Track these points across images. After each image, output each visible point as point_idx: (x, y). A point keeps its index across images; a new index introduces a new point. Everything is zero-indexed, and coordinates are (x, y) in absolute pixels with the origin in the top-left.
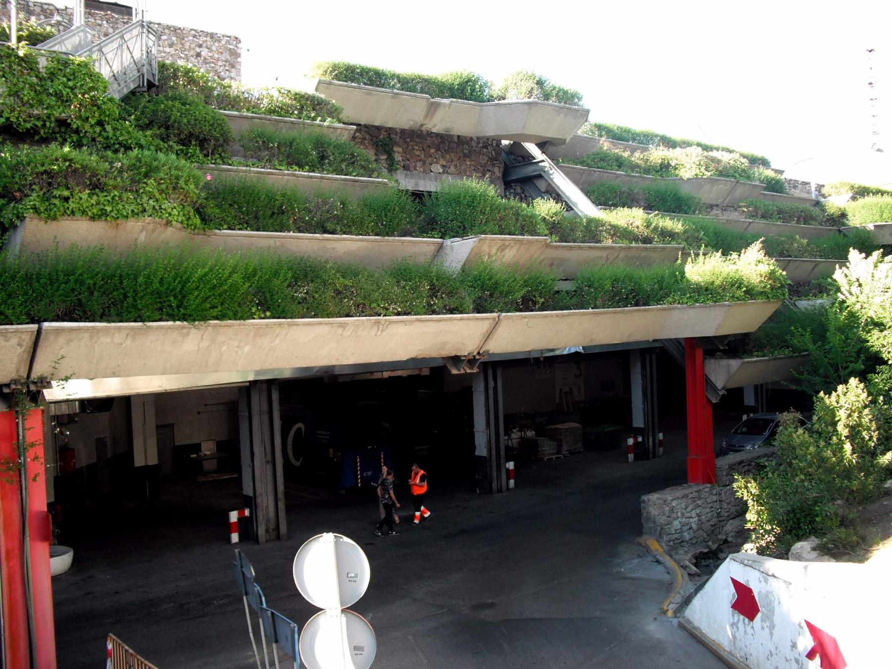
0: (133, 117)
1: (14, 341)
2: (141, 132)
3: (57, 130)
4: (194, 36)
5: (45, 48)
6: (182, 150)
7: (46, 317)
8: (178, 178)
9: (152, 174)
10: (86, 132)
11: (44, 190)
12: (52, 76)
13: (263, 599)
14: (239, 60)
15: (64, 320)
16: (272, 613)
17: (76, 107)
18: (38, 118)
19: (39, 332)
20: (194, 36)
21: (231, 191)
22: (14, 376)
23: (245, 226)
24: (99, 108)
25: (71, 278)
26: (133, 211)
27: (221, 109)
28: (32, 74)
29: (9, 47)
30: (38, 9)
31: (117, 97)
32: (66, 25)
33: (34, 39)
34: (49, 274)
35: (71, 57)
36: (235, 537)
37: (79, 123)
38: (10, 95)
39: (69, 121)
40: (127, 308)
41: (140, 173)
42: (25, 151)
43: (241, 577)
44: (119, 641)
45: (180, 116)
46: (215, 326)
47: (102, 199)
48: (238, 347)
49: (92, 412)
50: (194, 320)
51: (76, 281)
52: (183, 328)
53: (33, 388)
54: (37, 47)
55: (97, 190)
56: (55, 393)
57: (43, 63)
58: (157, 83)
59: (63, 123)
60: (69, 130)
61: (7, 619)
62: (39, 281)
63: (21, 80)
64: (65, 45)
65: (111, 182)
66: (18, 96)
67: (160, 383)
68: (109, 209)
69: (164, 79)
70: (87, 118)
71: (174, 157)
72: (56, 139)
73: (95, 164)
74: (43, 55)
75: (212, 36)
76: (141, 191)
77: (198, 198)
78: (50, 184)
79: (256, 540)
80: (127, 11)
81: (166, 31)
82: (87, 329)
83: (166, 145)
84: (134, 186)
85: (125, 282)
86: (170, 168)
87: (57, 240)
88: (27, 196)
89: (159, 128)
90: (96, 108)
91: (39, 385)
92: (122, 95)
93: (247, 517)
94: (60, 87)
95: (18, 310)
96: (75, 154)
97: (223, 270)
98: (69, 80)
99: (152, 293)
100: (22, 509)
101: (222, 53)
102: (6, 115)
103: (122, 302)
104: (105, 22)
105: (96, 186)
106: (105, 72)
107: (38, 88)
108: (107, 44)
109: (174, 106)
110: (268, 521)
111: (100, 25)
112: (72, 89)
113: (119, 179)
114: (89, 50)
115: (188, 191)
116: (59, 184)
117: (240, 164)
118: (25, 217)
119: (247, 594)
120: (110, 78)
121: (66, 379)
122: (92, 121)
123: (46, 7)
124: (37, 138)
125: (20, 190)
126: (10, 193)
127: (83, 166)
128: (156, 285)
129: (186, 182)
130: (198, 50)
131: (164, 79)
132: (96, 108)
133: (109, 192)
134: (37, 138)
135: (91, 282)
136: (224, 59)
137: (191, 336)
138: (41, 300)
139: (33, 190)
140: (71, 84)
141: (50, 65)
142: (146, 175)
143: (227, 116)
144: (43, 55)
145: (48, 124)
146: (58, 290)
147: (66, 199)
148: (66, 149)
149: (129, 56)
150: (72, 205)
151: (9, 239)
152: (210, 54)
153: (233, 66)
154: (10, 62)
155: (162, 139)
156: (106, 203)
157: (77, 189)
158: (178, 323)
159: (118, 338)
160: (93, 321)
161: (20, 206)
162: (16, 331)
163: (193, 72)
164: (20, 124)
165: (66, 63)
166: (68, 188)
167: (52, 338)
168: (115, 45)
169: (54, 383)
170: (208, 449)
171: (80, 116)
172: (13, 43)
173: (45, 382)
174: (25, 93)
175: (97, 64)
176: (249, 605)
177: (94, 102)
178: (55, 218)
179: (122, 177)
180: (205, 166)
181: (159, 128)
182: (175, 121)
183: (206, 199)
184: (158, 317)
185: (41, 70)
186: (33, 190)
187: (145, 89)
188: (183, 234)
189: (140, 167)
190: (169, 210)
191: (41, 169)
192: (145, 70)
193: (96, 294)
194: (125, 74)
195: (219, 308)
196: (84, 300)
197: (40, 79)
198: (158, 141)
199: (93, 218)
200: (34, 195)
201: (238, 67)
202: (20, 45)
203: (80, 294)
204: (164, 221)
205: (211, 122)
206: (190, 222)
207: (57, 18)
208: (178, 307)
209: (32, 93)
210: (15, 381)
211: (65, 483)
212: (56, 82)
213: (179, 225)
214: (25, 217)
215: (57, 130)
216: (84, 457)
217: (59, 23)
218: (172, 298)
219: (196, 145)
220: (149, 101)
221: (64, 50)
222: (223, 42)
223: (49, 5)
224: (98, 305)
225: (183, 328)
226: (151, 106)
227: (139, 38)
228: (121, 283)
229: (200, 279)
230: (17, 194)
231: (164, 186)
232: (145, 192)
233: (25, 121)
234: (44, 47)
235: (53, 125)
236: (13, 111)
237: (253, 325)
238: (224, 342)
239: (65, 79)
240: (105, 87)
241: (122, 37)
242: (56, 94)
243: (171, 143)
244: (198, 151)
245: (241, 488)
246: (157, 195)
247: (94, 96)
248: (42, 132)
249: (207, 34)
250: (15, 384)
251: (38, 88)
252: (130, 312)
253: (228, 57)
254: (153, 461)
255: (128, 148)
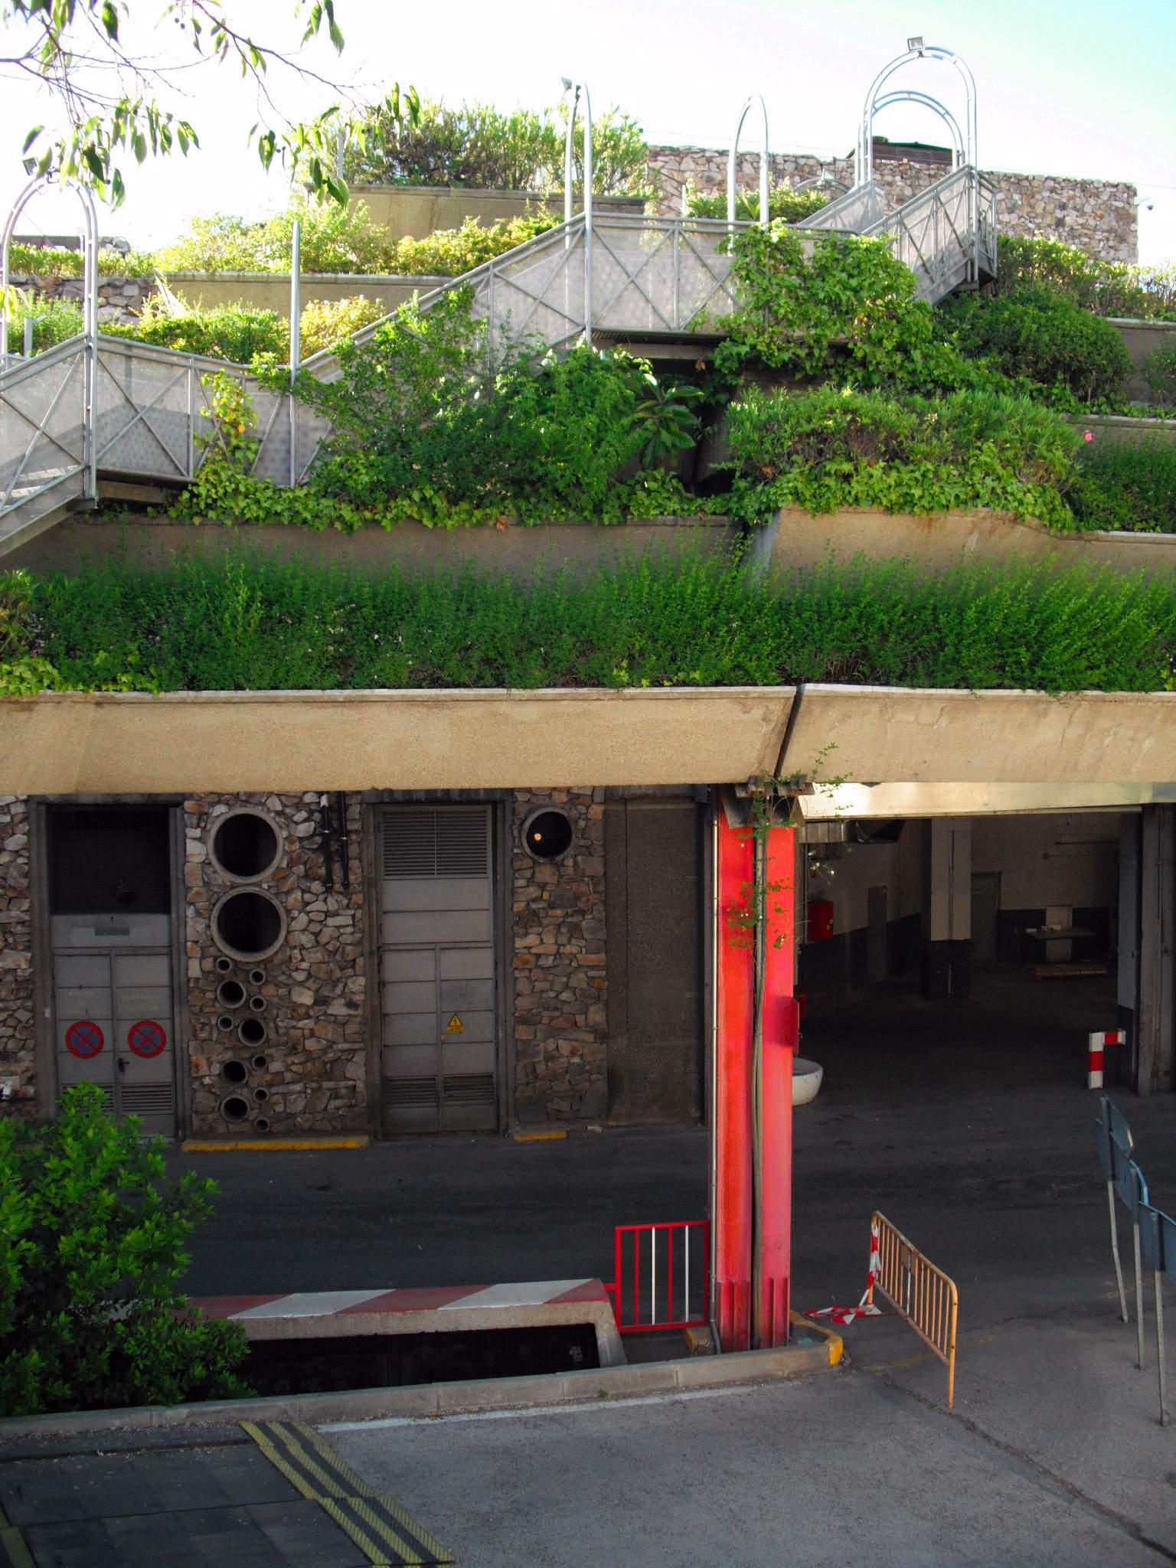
0: (955, 335)
1: (758, 713)
2: (969, 361)
3: (831, 361)
4: (1053, 190)
5: (811, 225)
6: (1040, 390)
7: (809, 675)
8: (1035, 439)
9: (991, 433)
10: (878, 364)
11: (811, 463)
12: (823, 271)
13: (1145, 1190)
14: (1133, 227)
15: (838, 682)
16: (1160, 1216)
17: (861, 321)
18: (801, 343)
19: (798, 698)
20: (1053, 190)
21: (1128, 463)
22: (754, 770)
23: (1152, 523)
24: (899, 322)
25: (853, 610)
26: (957, 496)
27: (1108, 315)
28: (792, 270)
29: (755, 230)
30: (790, 167)
31: (929, 301)
32: (840, 187)
33: (793, 214)
34: (818, 604)
35: (853, 237)
36: (1096, 1079)
37: (867, 348)
38: (757, 308)
39: (850, 346)
40: (944, 664)
41: (969, 432)
42: (781, 396)
43: (1108, 1147)
44: (890, 1224)
45: (1038, 330)
46: (1095, 700)
47: (906, 477)
48: (1132, 739)
49: (866, 842)
50: (1058, 689)
51: (860, 617)
52: (1038, 701)
53: (783, 792)
54: (799, 225)
55: (897, 461)
56: (816, 804)
57: (809, 250)
58: (995, 274)
59: (841, 350)
60: (850, 360)
61: (722, 1162)
62: (799, 615)
63: (774, 281)
64: (843, 217)
65: (923, 447)
66: (770, 308)
67: (986, 799)
68: (917, 492)
69: (1008, 267)
70: (880, 341)
71: (1026, 401)
72: (829, 377)
73: (894, 418)
74: (808, 238)
75: (1084, 186)
76: (972, 462)
77: (1069, 474)
78: (820, 452)
79: (1134, 1089)
80: (940, 156)
81: (1003, 184)
82: (876, 698)
83: (1012, 382)
84: (960, 456)
85: (942, 619)
86: (1020, 422)
87: (832, 546)
88: (782, 472)
89: (1000, 353)
90: (894, 322)
91: (794, 787)
92: (937, 298)
93: (1120, 1046)
94: (837, 289)
95: (765, 663)
96: (861, 401)
97: (1113, 602)
98: (851, 276)
99: (987, 641)
100: (754, 991)
101: (1102, 217)
102: (750, 340)
103: (935, 653)
104: (898, 178)
105: (896, 455)
106: (909, 259)
107: (801, 293)
108: (913, 211)
109: (1026, 313)
110: (1157, 1056)
111: (890, 184)
112: (856, 291)
113: (935, 442)
114: (883, 224)
115: (1052, 462)
116: (834, 452)
117: (1143, 413)
118: (779, 509)
119: (1114, 1177)
120: (917, 269)
121: (837, 782)
122: (888, 345)
123: (802, 162)
124: (798, 376)
125: (772, 464)
126: (757, 468)
127: (874, 422)
128: (995, 627)
129: (1050, 445)
130: (1059, 214)
131: (1008, 267)
132: (894, 322)
133: (917, 464)
134: (798, 376)
135: (886, 618)
136: (1105, 227)
137: (1052, 715)
138: (803, 647)
139: (793, 463)
140: (854, 282)
141: (820, 253)
142: (980, 435)
143: (1119, 327)
144: (808, 238)
145: (816, 352)
146: (830, 631)
147: (847, 478)
148: (847, 392)
149: (949, 230)
150: (856, 487)
151: (753, 546)
152: (1081, 221)
153: (1122, 239)
154: (758, 253)
155: (1006, 372)
156: (912, 483)
157: (864, 461)
158: (1030, 692)
159: (927, 715)
160: (887, 684)
161: (773, 490)
162: (762, 697)
163: (1059, 251)
164: (772, 355)
165: (846, 247)
166: (849, 459)
167: (817, 710)
168: (926, 211)
169: (816, 787)
170: (1057, 920)
171: (869, 337)
172: (762, 223)
173: (802, 784)
174: (782, 302)
175: (895, 246)
176: (1117, 1199)
177: (891, 313)
178: (827, 510)
179: (939, 439)
180: (1081, 418)
181: (1000, 353)
182: (1028, 340)
183: (1083, 475)
184: (996, 682)
185: (806, 263)
186: (793, 463)
187: (976, 286)
188: (1044, 538)
189: (970, 421)
190: (1020, 496)
191: (807, 428)
192: (975, 252)
193: (893, 637)
194: (942, 261)
195: (1103, 669)
196: (872, 648)
197: (805, 278)
198: (998, 376)
199: (889, 510)
200: (796, 471)
201: (1131, 240)
202: (774, 223)
203: (866, 637)
204: (1011, 514)
205: (1092, 339)
206: (1055, 516)
207: (827, 175)
208: (1033, 664)
209: (792, 303)
210: (755, 780)
211: (818, 952)
212: (831, 281)
213: (1036, 522)
214: (779, 509)
215: (831, 361)
216: (846, 920)
217: (827, 185)
218: (1022, 650)
219: (1064, 381)
220: (982, 307)
221: (840, 227)
222: (1105, 197)
223: (808, 157)
224: (896, 656)
225: (1038, 701)
226: (986, 315)
227: (965, 197)
228: (936, 620)
229: (1072, 616)
230: (768, 470)
231: (1010, 454)
232: (978, 465)
233: (779, 350)
234: (810, 226)
235: (824, 353)
236: (760, 333)
237: (1162, 701)
238: (1108, 730)
239: (844, 275)
240: (910, 286)
241: (937, 198)
242: (830, 301)
243: (1021, 378)
244: (1068, 392)
245: (1115, 995)
246: (998, 468)
247: (890, 301)
248: (808, 366)
249: (1074, 184)
250: (755, 784)
251: (801, 293)
252: (949, 672)
253: (1114, 223)
254: (962, 932)
255: (948, 389)
